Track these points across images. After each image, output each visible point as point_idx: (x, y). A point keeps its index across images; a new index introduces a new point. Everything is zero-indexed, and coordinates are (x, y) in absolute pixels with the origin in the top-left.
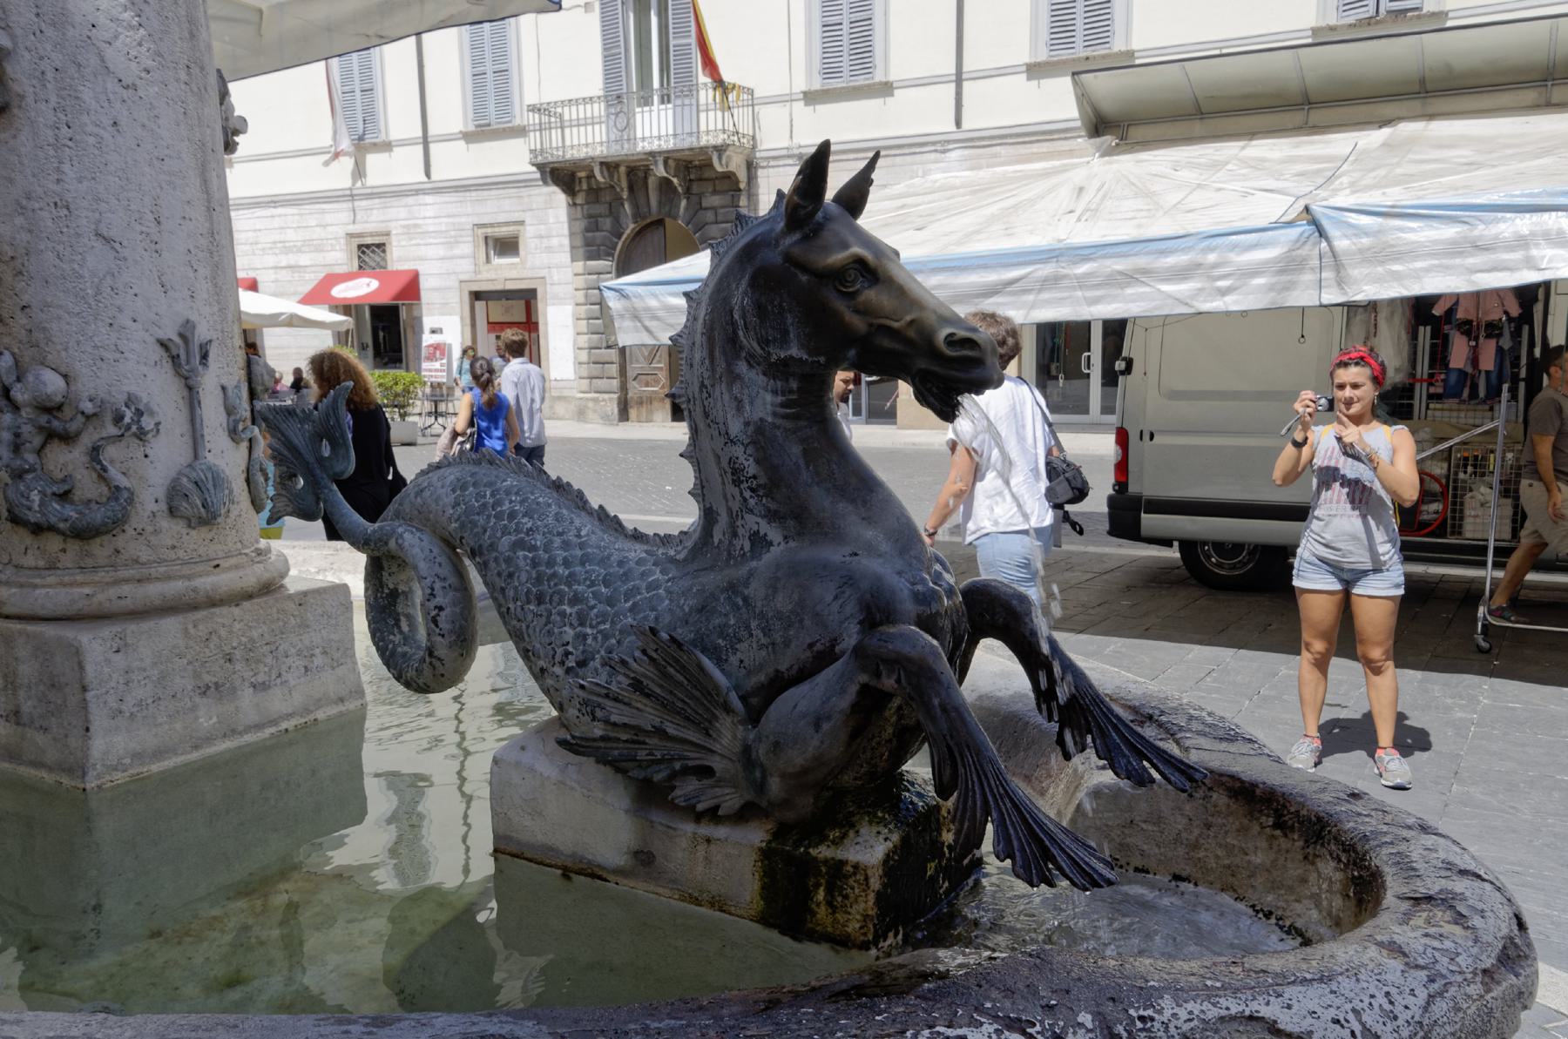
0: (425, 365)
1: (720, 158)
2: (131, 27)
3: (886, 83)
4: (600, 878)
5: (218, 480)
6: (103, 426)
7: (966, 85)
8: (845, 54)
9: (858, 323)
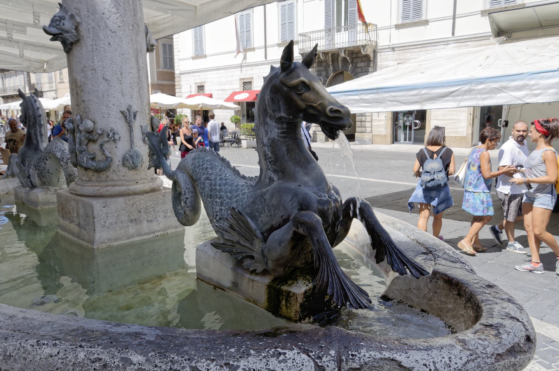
2: (115, 13)
3: (426, 20)
4: (223, 290)
5: (138, 156)
6: (104, 138)
7: (457, 20)
8: (411, 11)
9: (302, 105)
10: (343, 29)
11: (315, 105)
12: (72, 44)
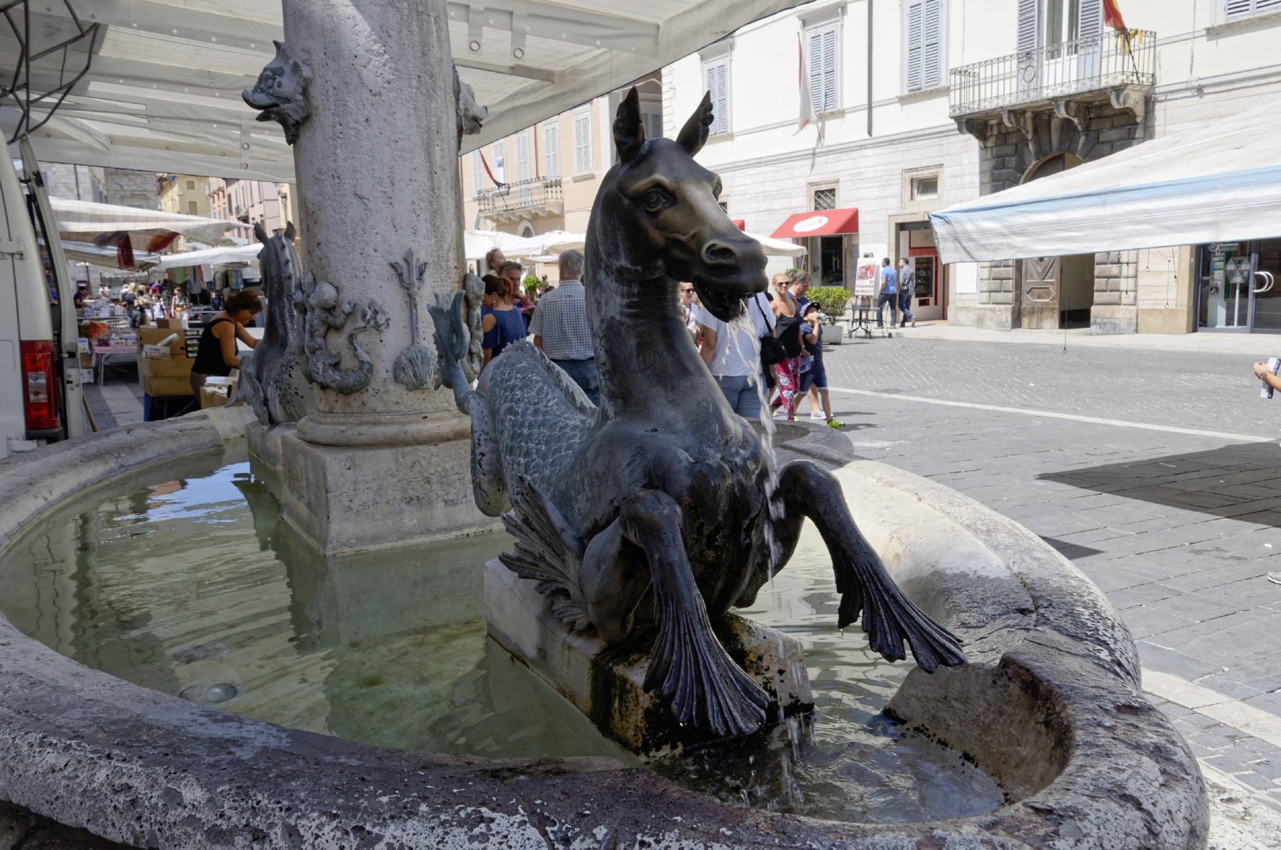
0: (858, 282)
1: (1118, 97)
2: (379, 54)
4: (524, 663)
9: (657, 237)
10: (1064, 50)
11: (683, 238)
12: (298, 124)
